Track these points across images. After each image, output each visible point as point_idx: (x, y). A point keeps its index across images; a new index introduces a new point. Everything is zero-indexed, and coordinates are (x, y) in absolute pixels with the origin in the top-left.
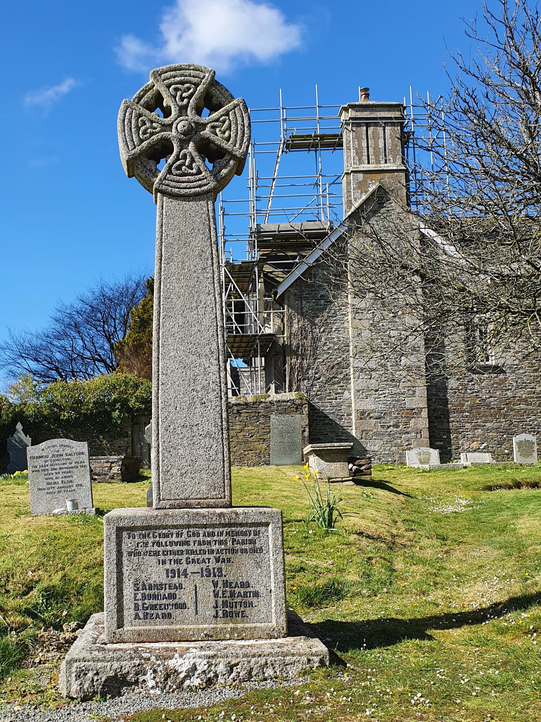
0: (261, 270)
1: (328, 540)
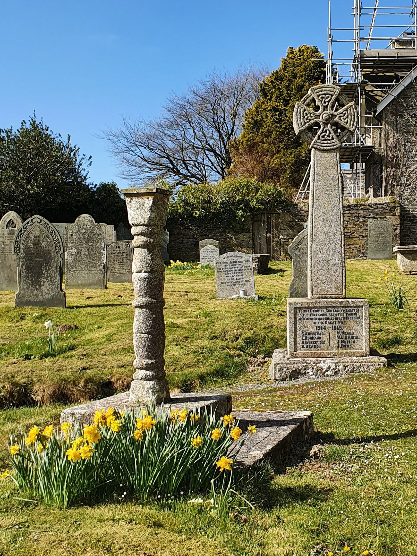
0: (363, 89)
1: (398, 316)
